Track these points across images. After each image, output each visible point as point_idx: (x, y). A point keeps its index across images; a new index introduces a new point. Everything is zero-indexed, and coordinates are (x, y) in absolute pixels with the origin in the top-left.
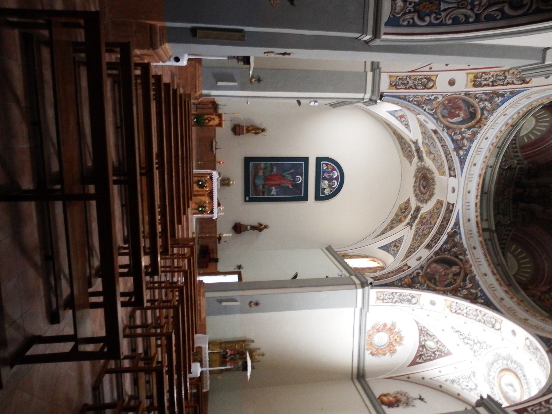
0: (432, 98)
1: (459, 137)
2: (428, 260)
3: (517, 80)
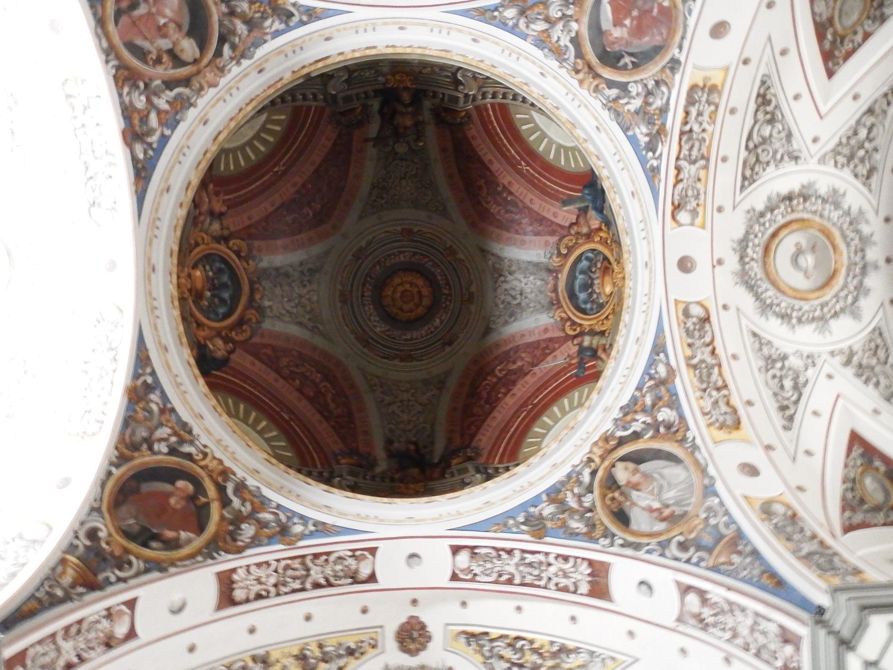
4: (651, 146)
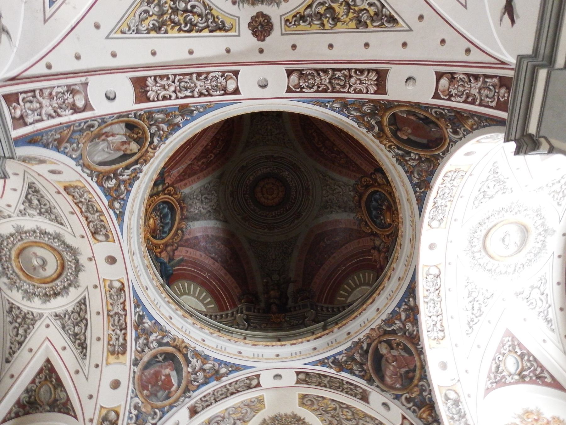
0: (135, 412)
1: (201, 375)
2: (382, 390)
3: (120, 299)
4: (141, 318)
